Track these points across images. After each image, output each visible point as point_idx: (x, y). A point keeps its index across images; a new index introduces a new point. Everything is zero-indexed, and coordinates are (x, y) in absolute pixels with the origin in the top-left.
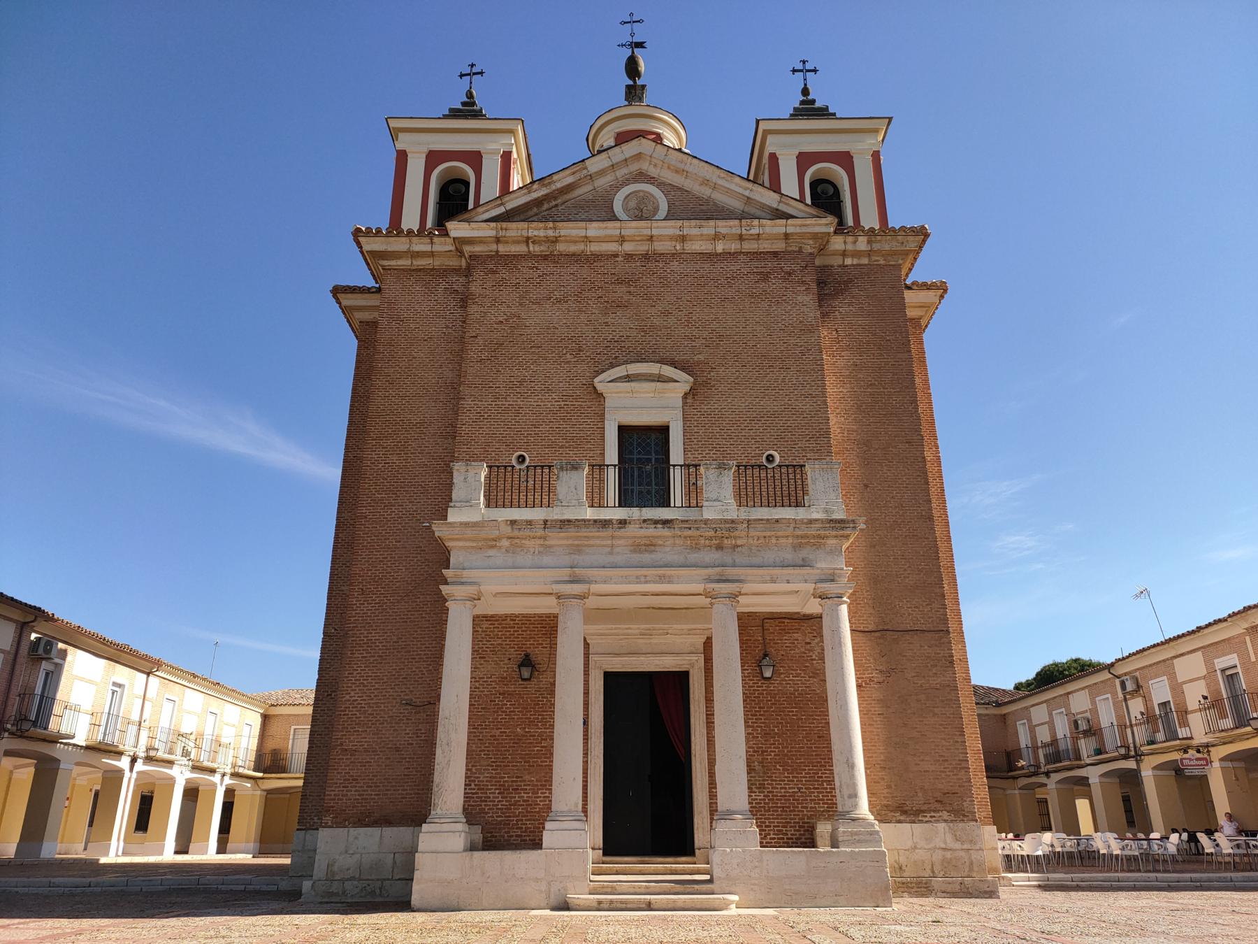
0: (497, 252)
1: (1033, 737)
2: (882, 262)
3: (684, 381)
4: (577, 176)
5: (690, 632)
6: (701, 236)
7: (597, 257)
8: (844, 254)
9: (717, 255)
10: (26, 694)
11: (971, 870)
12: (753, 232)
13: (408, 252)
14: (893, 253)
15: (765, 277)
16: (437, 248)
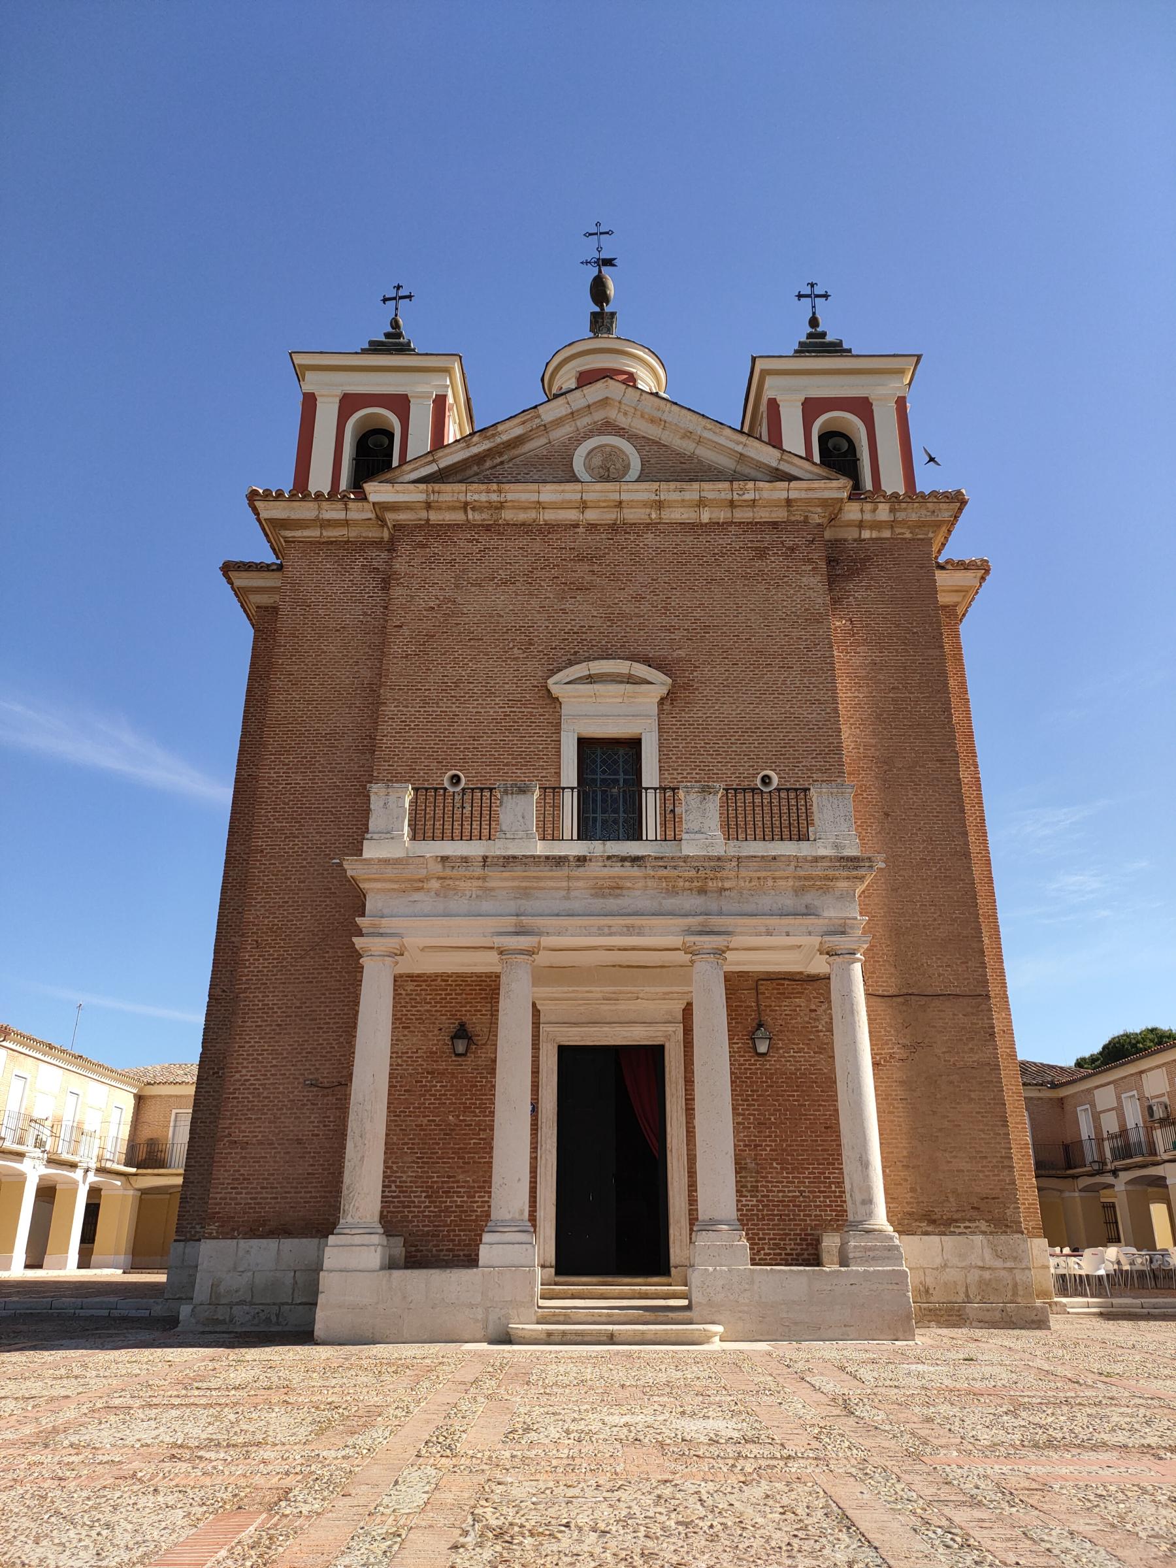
0: (428, 520)
1: (1098, 1127)
2: (908, 535)
3: (660, 683)
4: (528, 426)
6: (681, 502)
7: (552, 528)
8: (861, 525)
9: (702, 525)
11: (1015, 1294)
12: (746, 497)
14: (922, 525)
15: (762, 553)
16: (353, 515)
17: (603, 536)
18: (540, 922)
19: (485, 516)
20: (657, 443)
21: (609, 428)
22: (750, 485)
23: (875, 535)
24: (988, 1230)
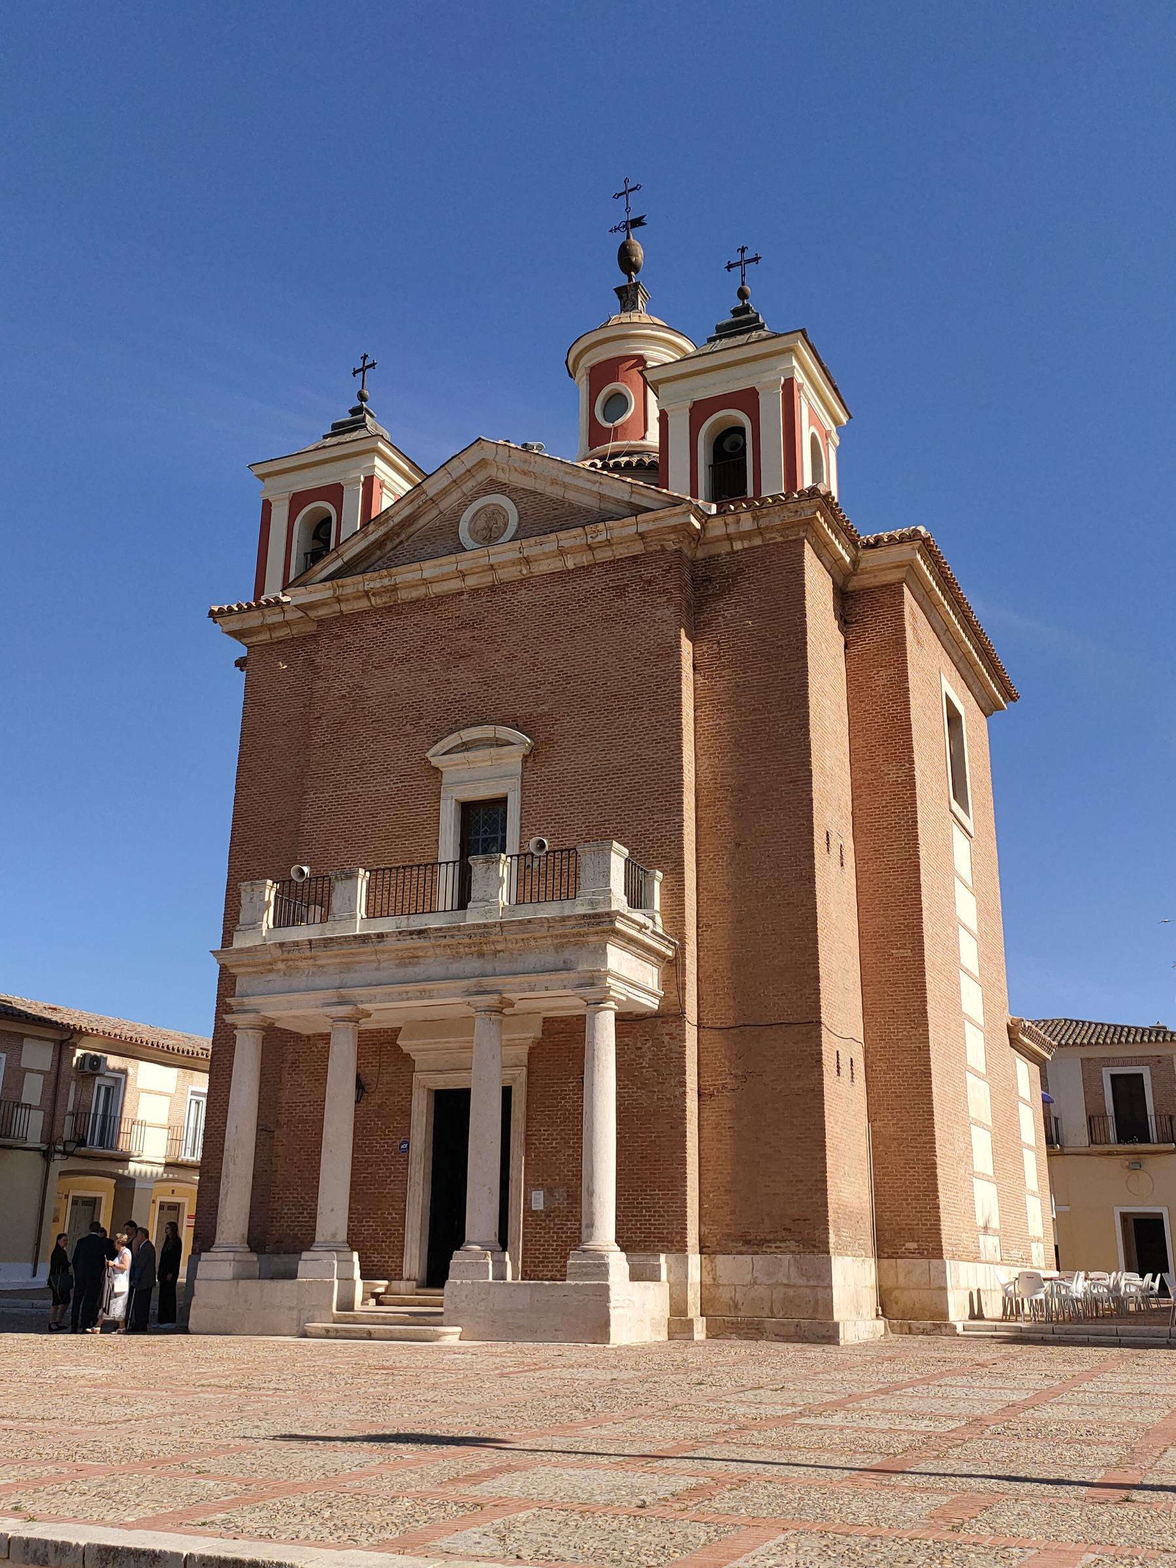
0: (341, 612)
2: (779, 539)
4: (416, 504)
6: (549, 553)
7: (442, 598)
8: (729, 538)
9: (570, 571)
10: (81, 1113)
11: (815, 1310)
13: (262, 625)
15: (621, 591)
20: (533, 493)
21: (494, 486)
22: (601, 526)
23: (746, 544)
24: (797, 1249)
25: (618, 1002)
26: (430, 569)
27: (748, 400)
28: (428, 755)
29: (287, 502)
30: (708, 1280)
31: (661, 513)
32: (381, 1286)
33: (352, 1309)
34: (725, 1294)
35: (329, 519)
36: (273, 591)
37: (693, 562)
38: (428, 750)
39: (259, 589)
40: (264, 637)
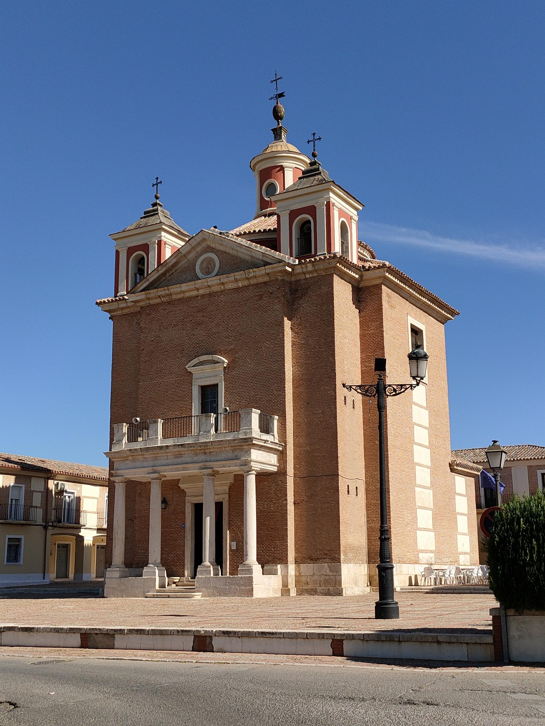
2: (324, 274)
4: (177, 258)
5: (221, 485)
6: (233, 281)
7: (190, 298)
8: (304, 273)
11: (335, 584)
12: (251, 275)
15: (261, 297)
17: (207, 299)
18: (158, 468)
19: (167, 299)
22: (251, 270)
25: (256, 471)
26: (184, 287)
27: (312, 210)
28: (186, 367)
29: (126, 251)
30: (298, 574)
31: (274, 266)
32: (177, 579)
33: (165, 588)
34: (303, 579)
35: (143, 258)
36: (123, 292)
37: (290, 283)
38: (187, 364)
39: (116, 291)
40: (119, 313)
